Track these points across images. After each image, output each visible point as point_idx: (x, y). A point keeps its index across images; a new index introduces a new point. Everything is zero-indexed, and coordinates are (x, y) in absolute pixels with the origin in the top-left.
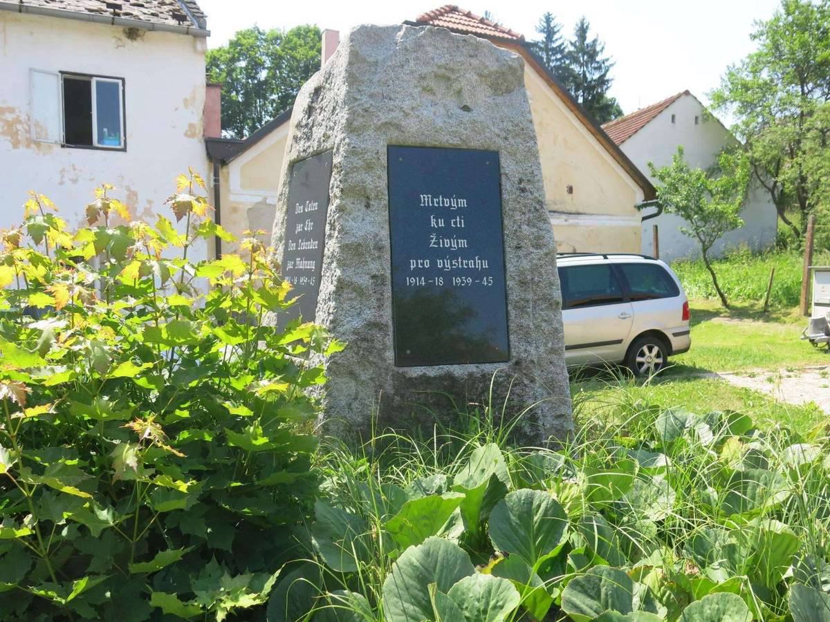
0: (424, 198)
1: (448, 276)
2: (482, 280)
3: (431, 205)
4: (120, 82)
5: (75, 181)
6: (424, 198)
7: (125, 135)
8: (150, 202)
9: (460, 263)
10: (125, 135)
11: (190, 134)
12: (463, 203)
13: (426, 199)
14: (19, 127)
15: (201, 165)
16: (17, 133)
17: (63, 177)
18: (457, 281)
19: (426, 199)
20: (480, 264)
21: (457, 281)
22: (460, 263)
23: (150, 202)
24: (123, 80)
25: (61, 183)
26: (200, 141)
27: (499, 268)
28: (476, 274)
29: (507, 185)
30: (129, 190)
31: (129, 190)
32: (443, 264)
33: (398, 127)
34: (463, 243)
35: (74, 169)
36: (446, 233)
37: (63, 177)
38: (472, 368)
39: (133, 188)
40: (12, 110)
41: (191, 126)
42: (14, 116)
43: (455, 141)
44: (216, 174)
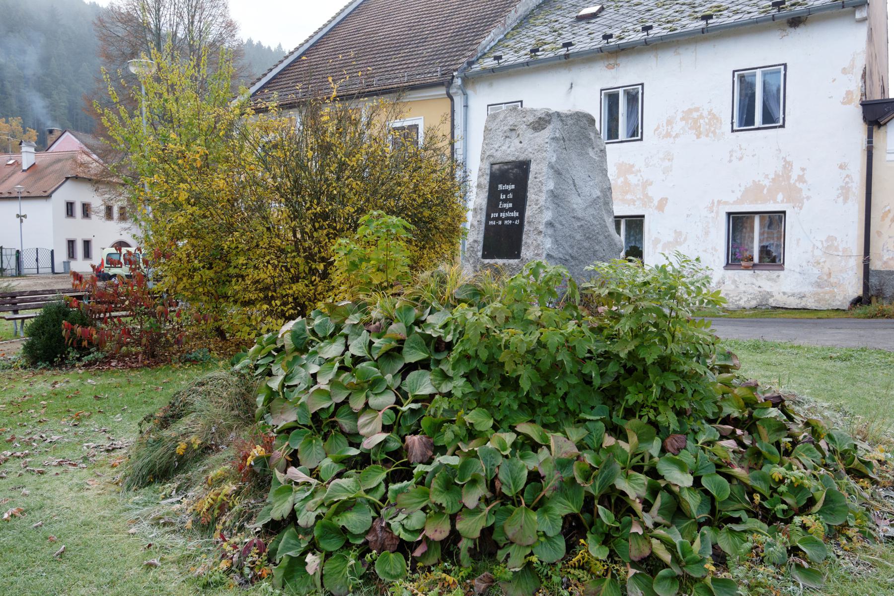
4: (736, 73)
5: (741, 159)
7: (784, 113)
8: (803, 169)
9: (509, 214)
10: (784, 113)
11: (847, 101)
12: (513, 187)
14: (702, 121)
15: (860, 130)
16: (700, 127)
17: (731, 156)
20: (515, 214)
21: (506, 222)
22: (509, 214)
23: (803, 169)
24: (734, 72)
25: (730, 161)
26: (857, 107)
27: (522, 217)
28: (513, 219)
29: (531, 176)
30: (785, 161)
31: (785, 161)
32: (503, 215)
33: (492, 156)
34: (511, 205)
35: (741, 149)
36: (505, 201)
37: (731, 156)
38: (505, 261)
39: (788, 159)
40: (697, 110)
41: (849, 93)
42: (699, 114)
43: (513, 159)
44: (870, 136)
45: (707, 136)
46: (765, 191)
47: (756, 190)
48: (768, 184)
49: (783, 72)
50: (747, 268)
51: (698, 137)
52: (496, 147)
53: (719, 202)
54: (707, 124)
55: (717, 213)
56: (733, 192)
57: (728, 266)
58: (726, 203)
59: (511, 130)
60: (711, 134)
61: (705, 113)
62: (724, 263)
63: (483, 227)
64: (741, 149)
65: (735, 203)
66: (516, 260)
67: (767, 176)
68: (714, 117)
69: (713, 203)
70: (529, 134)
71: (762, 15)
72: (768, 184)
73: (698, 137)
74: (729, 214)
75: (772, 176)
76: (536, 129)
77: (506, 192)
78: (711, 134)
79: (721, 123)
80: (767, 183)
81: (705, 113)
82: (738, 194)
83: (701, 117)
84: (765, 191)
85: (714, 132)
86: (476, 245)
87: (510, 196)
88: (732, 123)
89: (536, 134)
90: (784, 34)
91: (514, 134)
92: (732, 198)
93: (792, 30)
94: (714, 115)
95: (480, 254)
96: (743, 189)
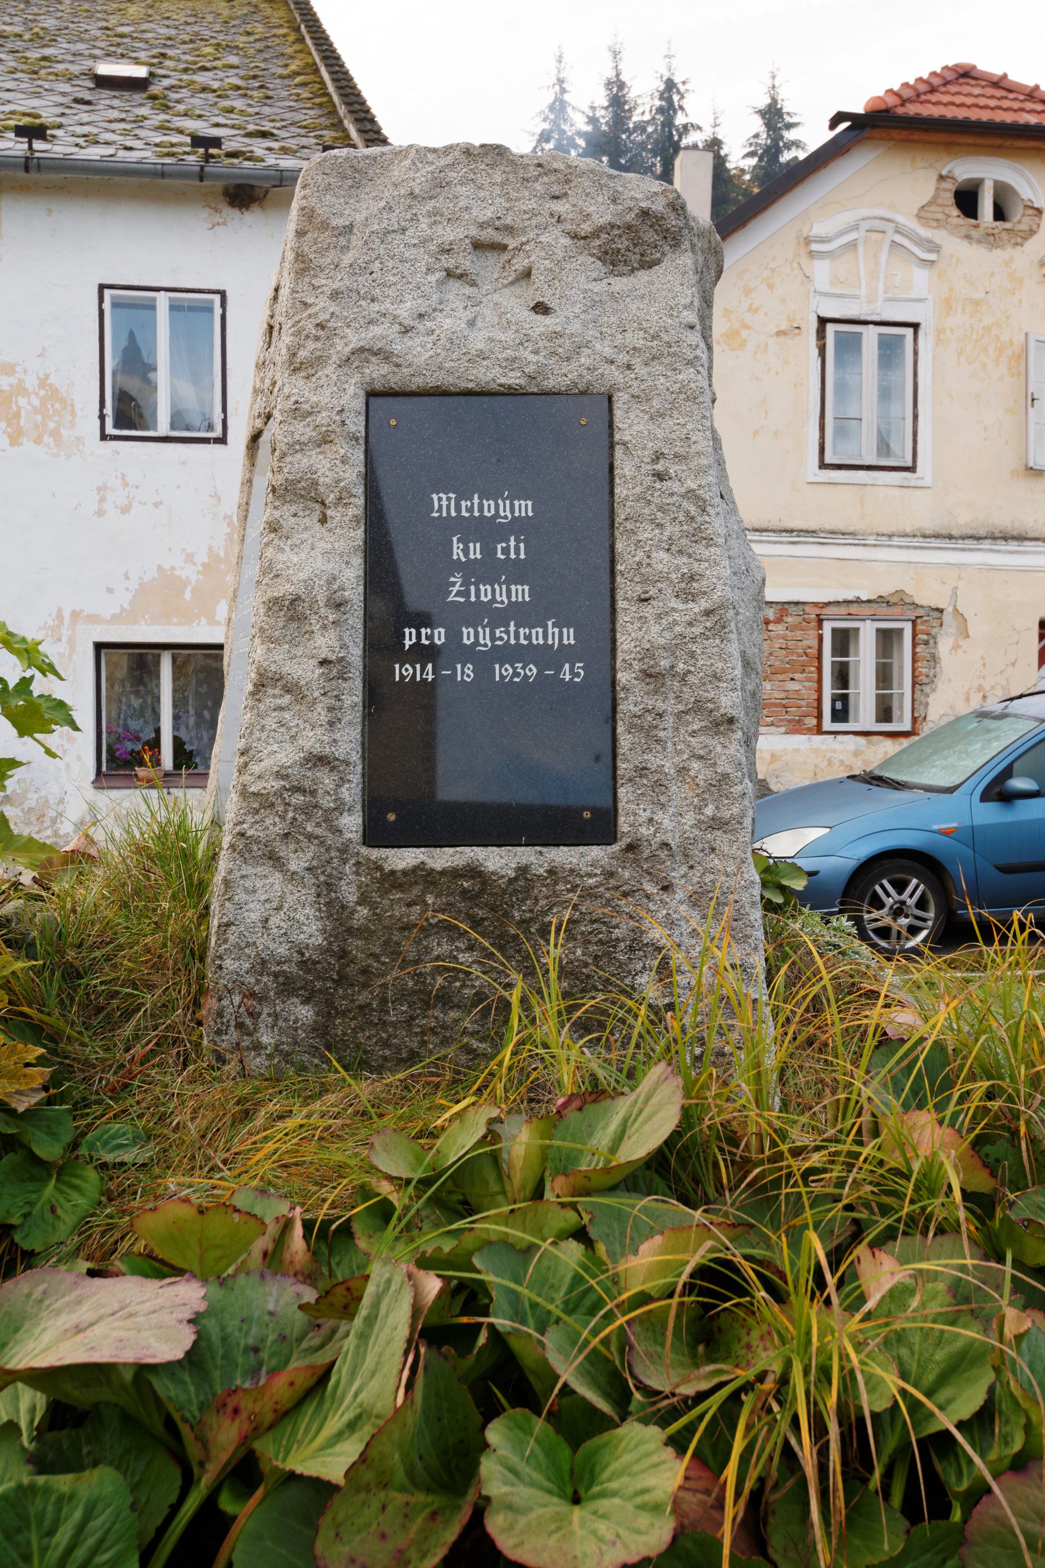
0: (440, 499)
1: (484, 661)
2: (559, 669)
3: (453, 514)
5: (126, 509)
6: (440, 499)
9: (510, 634)
12: (524, 508)
13: (444, 503)
14: (22, 401)
16: (17, 415)
17: (102, 500)
18: (503, 671)
19: (444, 503)
21: (503, 671)
22: (510, 634)
25: (100, 513)
33: (384, 355)
34: (521, 592)
35: (126, 485)
37: (102, 500)
42: (14, 381)
45: (38, 441)
46: (188, 595)
47: (163, 589)
48: (194, 578)
49: (218, 311)
50: (151, 784)
51: (14, 441)
52: (404, 311)
53: (75, 615)
54: (35, 411)
55: (72, 642)
56: (110, 591)
57: (103, 778)
58: (94, 619)
59: (478, 246)
60: (47, 439)
61: (31, 382)
62: (92, 776)
63: (353, 693)
64: (126, 485)
65: (115, 619)
66: (595, 852)
67: (190, 558)
68: (53, 396)
69: (60, 617)
70: (583, 279)
71: (167, 160)
72: (194, 578)
73: (14, 441)
74: (99, 647)
75: (202, 558)
76: (613, 260)
77: (487, 531)
78: (47, 439)
79: (73, 413)
80: (190, 573)
81: (31, 382)
82: (123, 599)
83: (20, 389)
84: (188, 595)
85: (56, 434)
86: (327, 780)
87: (515, 549)
88: (102, 417)
89: (620, 284)
90: (218, 219)
91: (489, 267)
92: (108, 607)
93: (235, 213)
94: (55, 391)
95: (352, 823)
96: (134, 585)
